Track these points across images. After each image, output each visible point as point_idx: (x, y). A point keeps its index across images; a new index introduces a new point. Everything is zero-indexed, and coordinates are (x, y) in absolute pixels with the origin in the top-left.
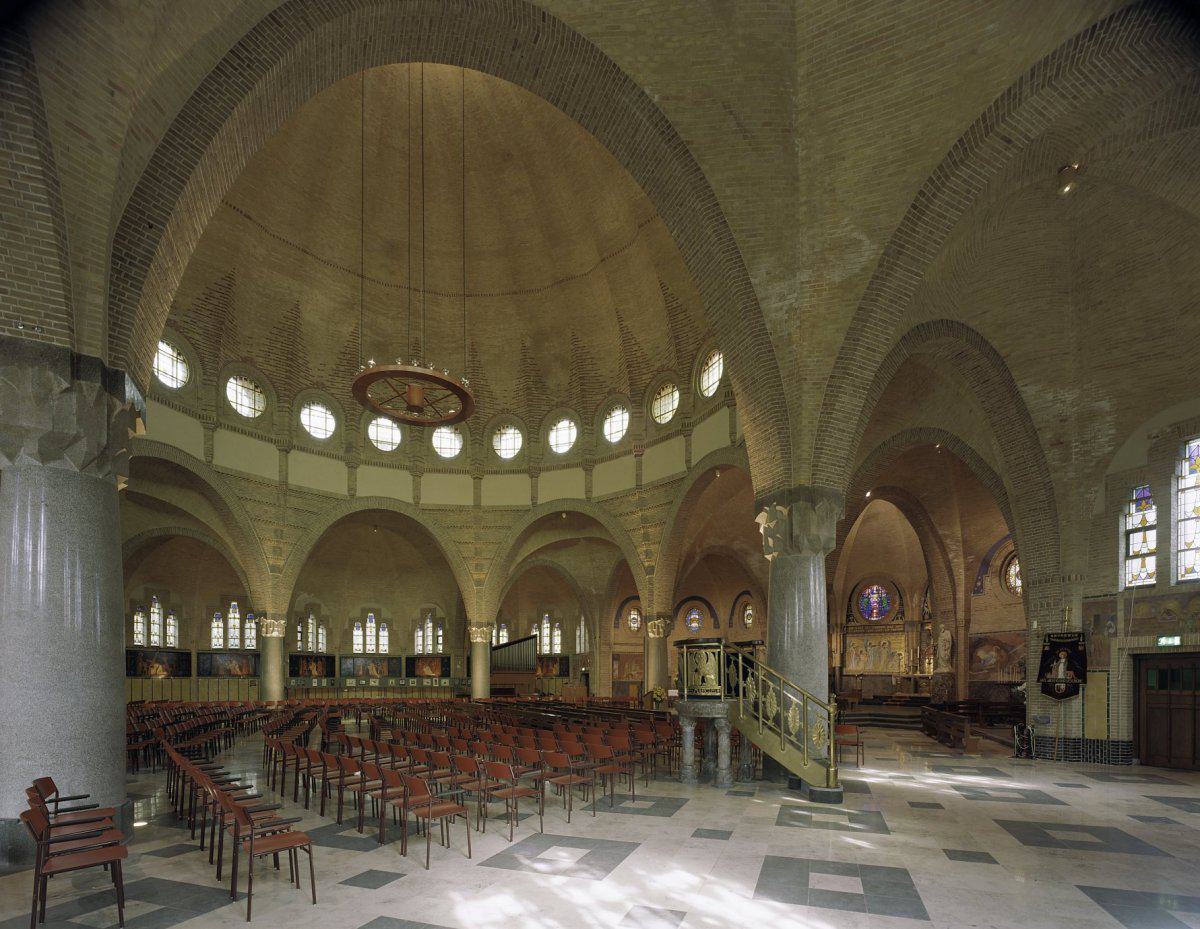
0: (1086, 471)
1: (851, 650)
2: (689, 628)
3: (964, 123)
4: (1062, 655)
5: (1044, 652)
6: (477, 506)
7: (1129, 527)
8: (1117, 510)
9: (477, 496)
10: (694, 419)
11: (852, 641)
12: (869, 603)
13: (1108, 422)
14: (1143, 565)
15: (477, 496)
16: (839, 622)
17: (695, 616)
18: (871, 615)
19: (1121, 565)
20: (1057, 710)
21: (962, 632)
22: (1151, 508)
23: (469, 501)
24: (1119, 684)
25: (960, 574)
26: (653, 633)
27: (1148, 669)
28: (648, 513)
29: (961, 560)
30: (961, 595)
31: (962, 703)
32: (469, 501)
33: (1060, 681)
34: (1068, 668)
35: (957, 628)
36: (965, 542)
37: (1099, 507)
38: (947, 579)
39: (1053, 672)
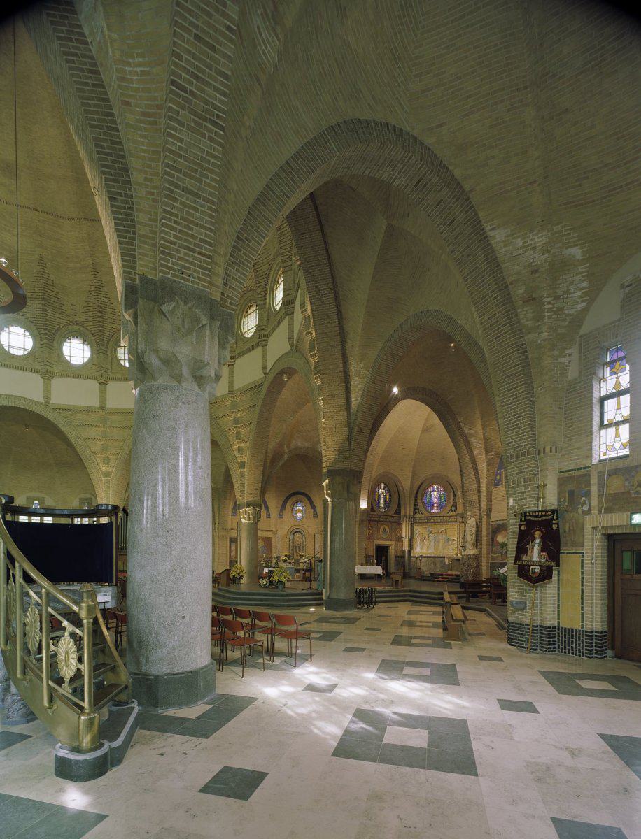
0: (559, 331)
1: (416, 536)
2: (295, 517)
3: (547, 255)
4: (537, 534)
5: (520, 531)
6: (103, 407)
7: (604, 393)
8: (589, 374)
9: (103, 399)
10: (269, 330)
11: (417, 528)
12: (431, 499)
13: (581, 273)
14: (617, 435)
15: (103, 399)
16: (408, 514)
17: (299, 507)
18: (432, 509)
19: (595, 434)
20: (532, 595)
21: (484, 519)
22: (625, 370)
23: (95, 403)
24: (593, 567)
25: (483, 468)
26: (244, 518)
27: (622, 552)
28: (239, 415)
29: (484, 456)
30: (484, 488)
31: (484, 582)
32: (95, 403)
33: (534, 564)
34: (542, 550)
35: (481, 515)
36: (486, 440)
37: (573, 372)
38: (472, 472)
39: (529, 552)
